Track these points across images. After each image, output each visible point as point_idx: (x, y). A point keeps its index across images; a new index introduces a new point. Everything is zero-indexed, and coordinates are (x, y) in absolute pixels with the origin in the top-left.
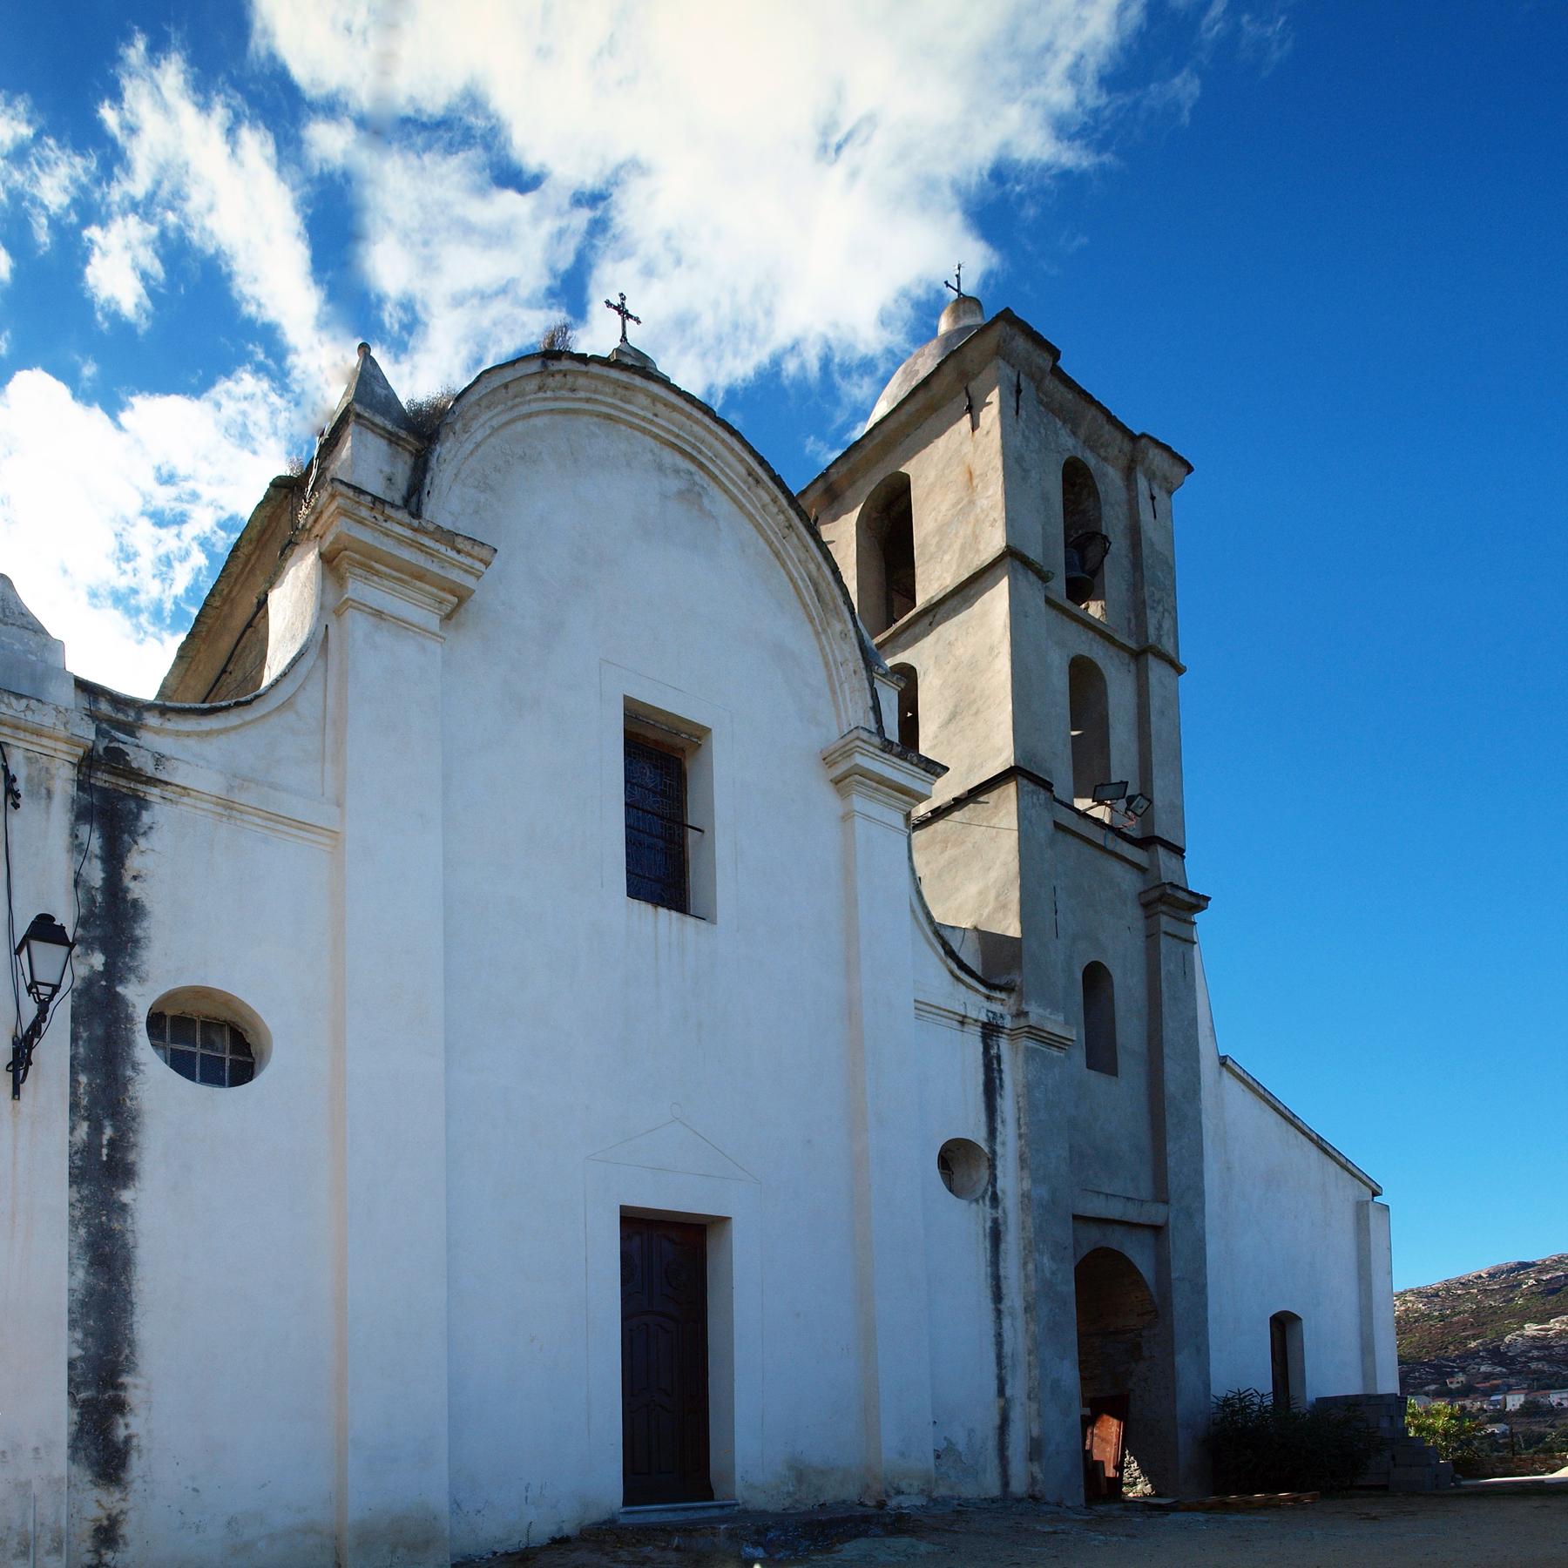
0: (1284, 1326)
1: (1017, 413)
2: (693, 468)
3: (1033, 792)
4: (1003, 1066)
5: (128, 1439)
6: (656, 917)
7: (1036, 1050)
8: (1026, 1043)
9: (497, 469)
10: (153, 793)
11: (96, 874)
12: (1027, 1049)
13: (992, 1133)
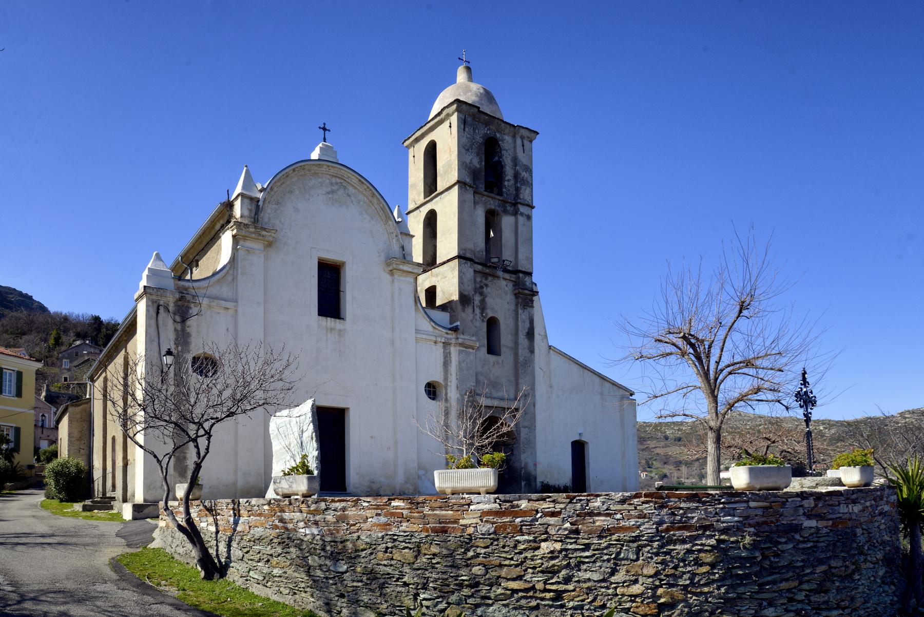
0: (579, 449)
1: (464, 130)
2: (342, 181)
3: (466, 263)
4: (452, 356)
5: (187, 466)
6: (327, 321)
7: (463, 351)
8: (458, 348)
9: (281, 197)
10: (192, 305)
11: (179, 327)
12: (459, 350)
13: (446, 379)
